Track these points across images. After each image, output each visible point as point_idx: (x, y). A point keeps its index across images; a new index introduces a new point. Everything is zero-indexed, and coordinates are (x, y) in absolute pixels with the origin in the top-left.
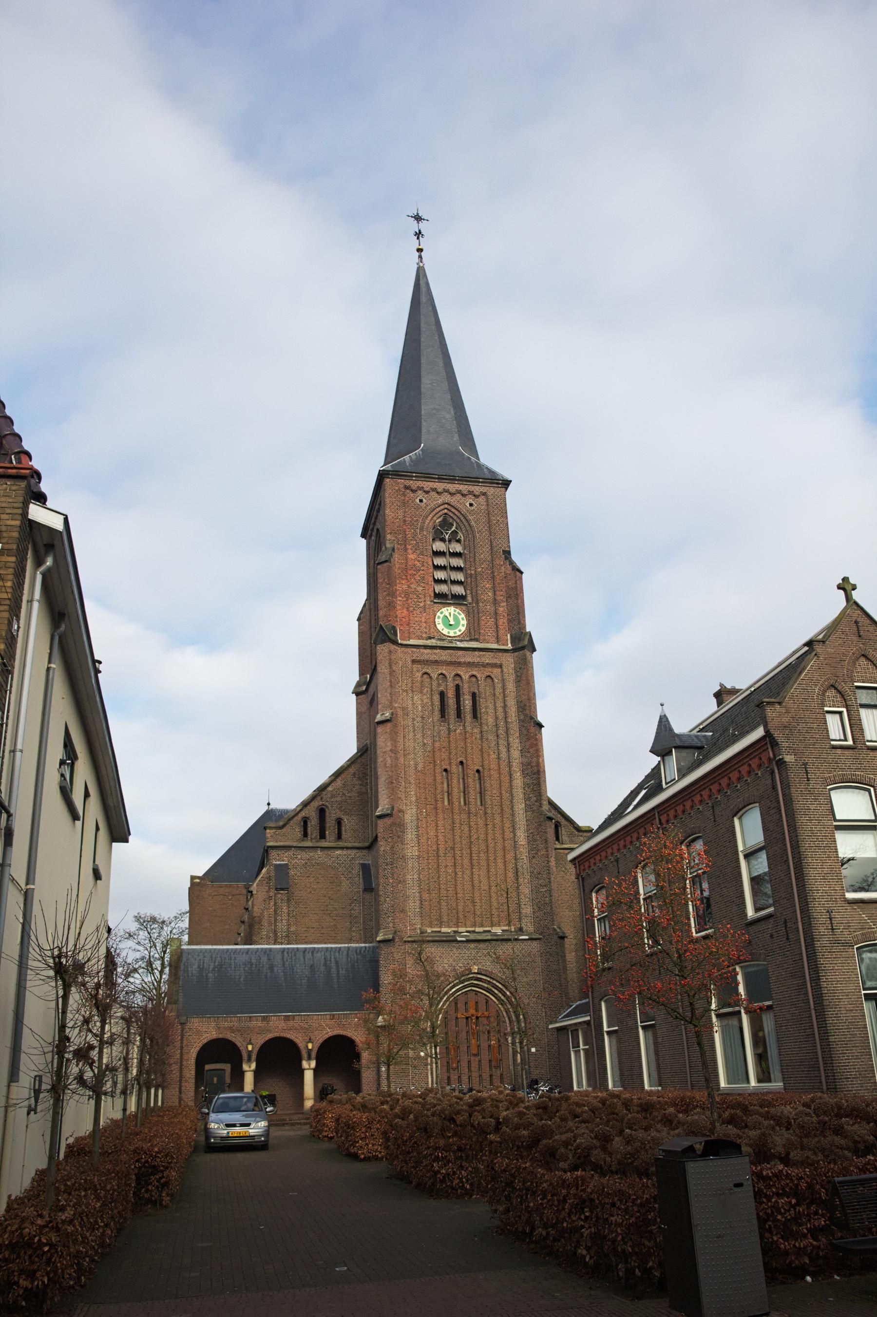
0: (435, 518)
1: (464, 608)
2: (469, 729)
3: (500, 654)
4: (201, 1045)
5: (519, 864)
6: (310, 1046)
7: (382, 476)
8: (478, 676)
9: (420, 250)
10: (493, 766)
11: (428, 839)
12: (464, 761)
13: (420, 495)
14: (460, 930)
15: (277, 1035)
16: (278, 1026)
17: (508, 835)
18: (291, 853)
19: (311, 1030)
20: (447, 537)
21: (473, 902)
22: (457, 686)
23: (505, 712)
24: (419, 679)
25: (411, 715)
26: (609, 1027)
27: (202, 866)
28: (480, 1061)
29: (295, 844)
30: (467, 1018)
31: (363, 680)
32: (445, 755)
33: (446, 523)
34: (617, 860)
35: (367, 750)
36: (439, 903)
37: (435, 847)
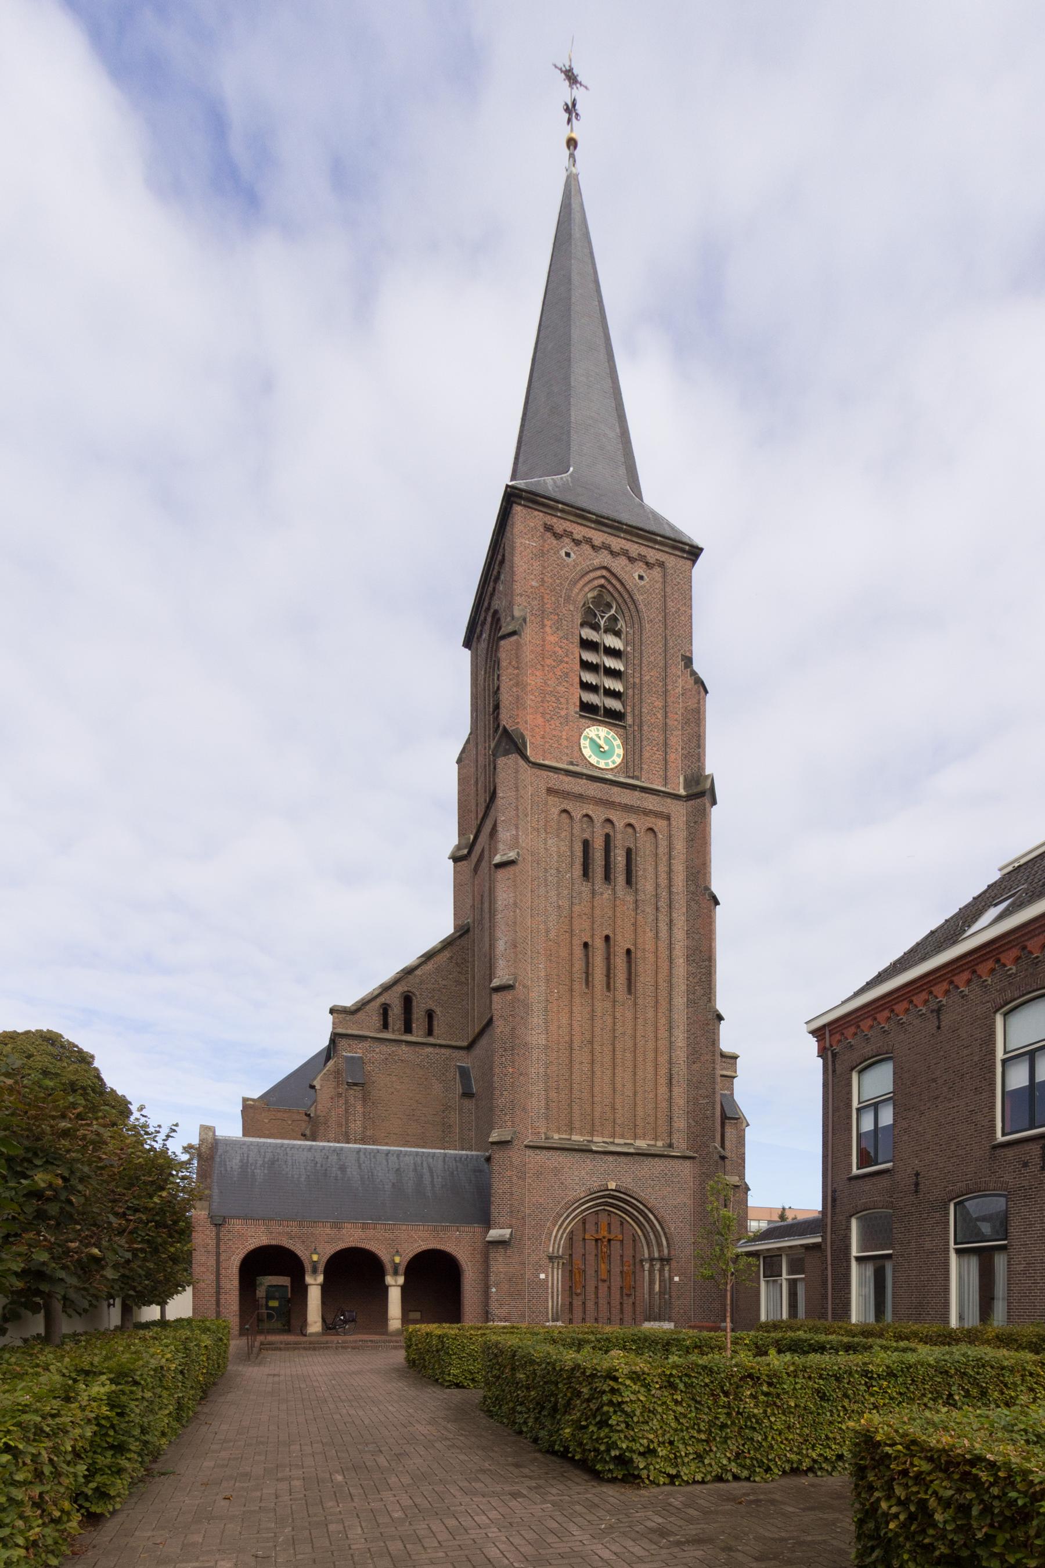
0: (586, 589)
1: (621, 731)
2: (620, 893)
3: (669, 800)
4: (245, 1252)
5: (675, 1070)
6: (397, 1260)
7: (512, 497)
8: (636, 826)
9: (572, 143)
10: (650, 946)
11: (559, 1027)
12: (612, 936)
13: (567, 546)
14: (596, 1139)
15: (353, 1245)
16: (352, 1237)
17: (663, 1033)
18: (366, 1044)
19: (397, 1245)
20: (602, 623)
21: (614, 1109)
22: (607, 837)
23: (670, 879)
24: (555, 816)
25: (543, 864)
26: (862, 1248)
27: (256, 1093)
28: (609, 1288)
29: (372, 1035)
30: (597, 1240)
31: (464, 842)
32: (586, 925)
33: (601, 602)
34: (938, 1011)
35: (468, 931)
36: (570, 1105)
37: (567, 1038)
